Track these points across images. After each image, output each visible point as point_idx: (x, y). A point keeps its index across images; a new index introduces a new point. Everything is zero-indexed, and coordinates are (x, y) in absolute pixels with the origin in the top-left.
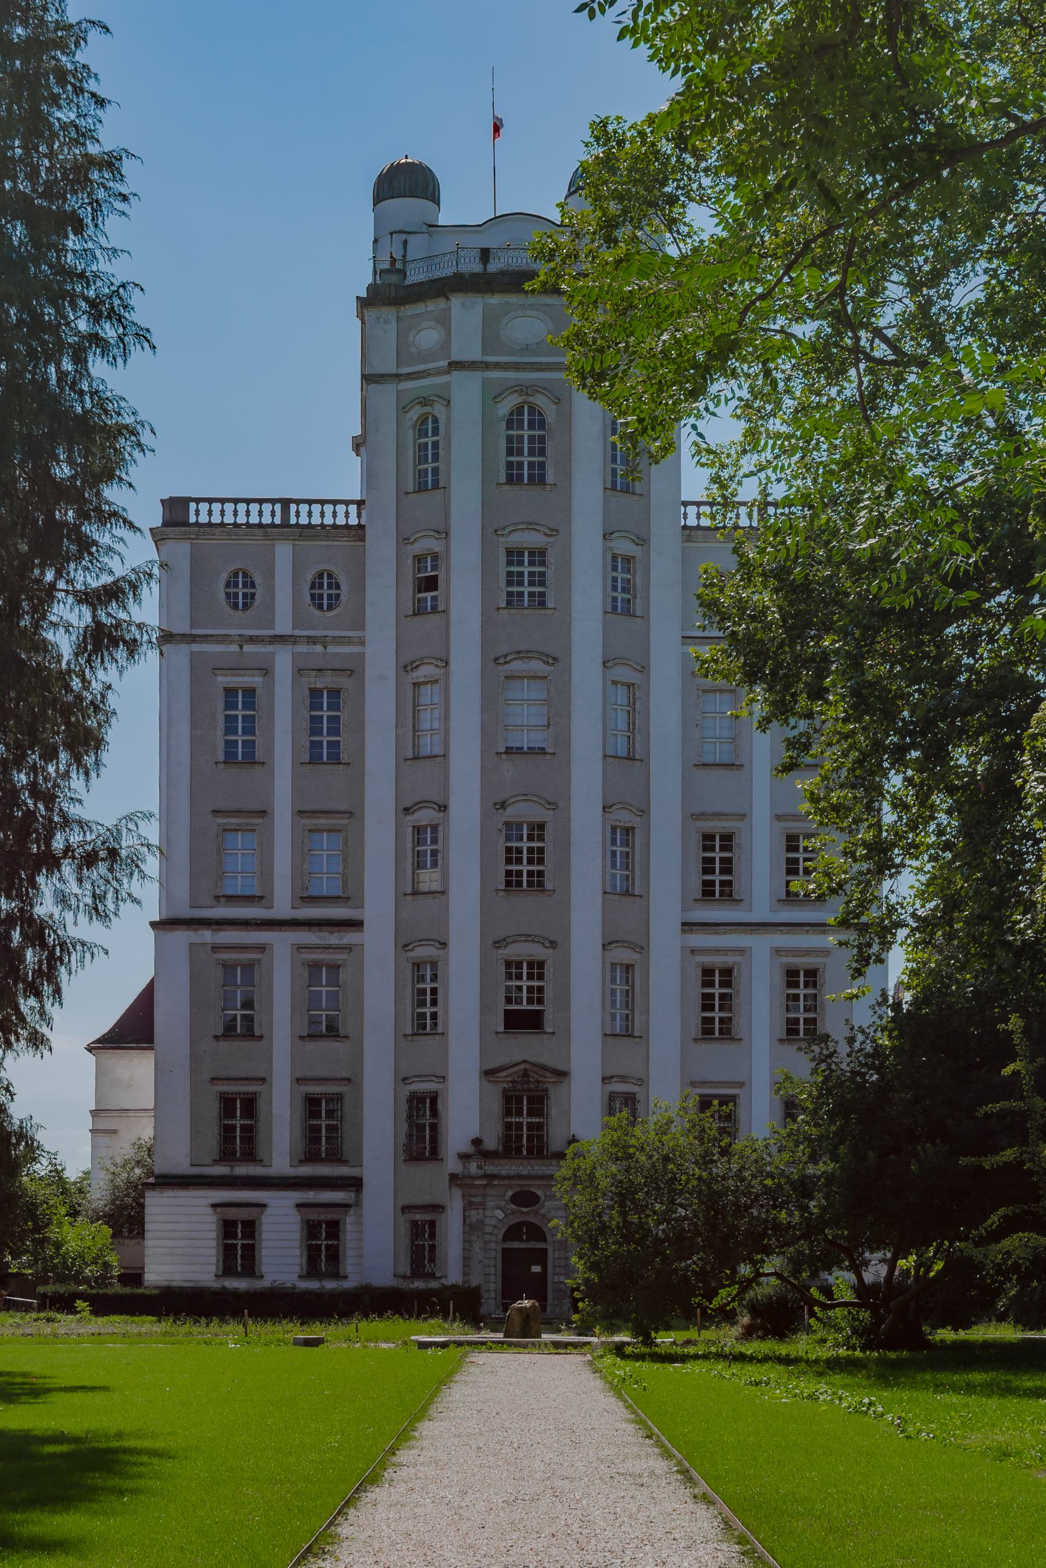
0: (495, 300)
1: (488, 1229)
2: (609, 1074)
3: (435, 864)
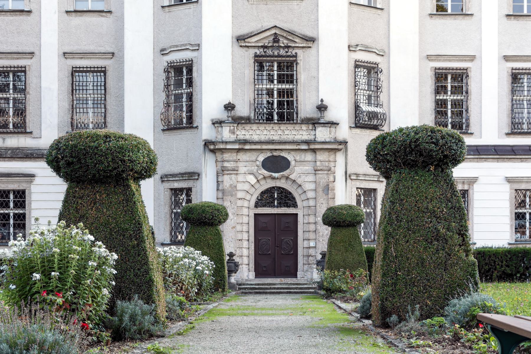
1: (240, 195)
2: (353, 43)
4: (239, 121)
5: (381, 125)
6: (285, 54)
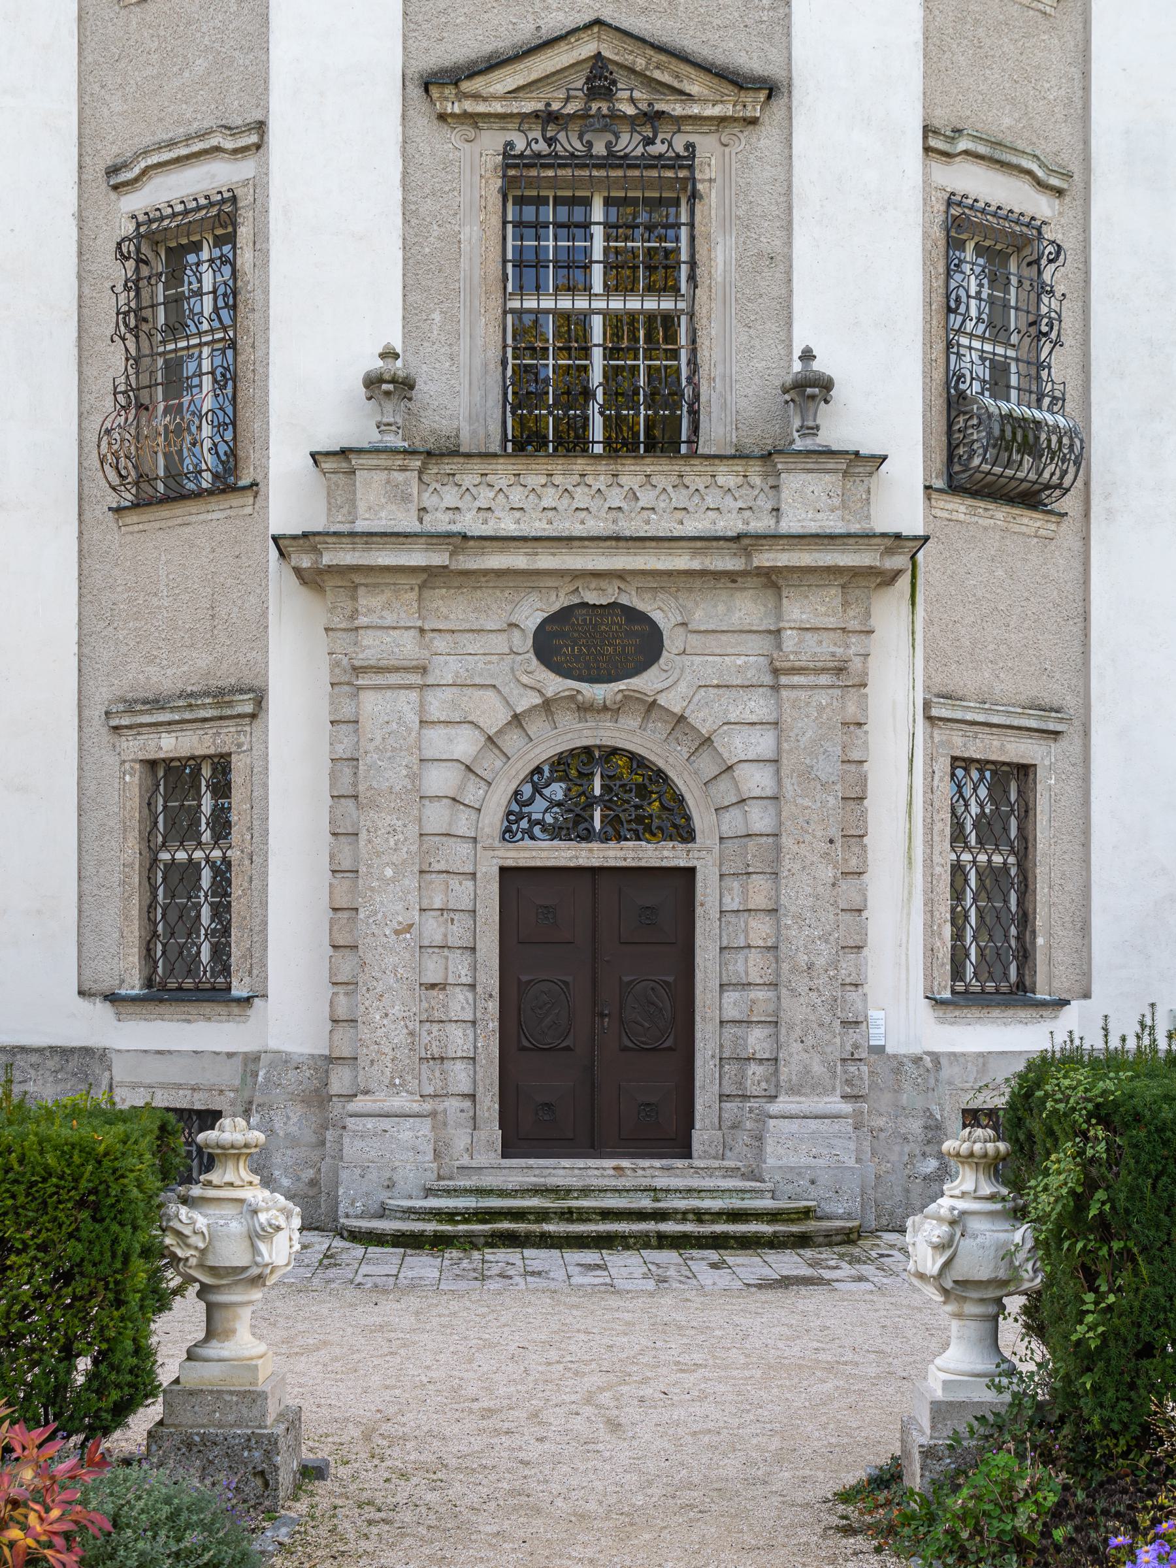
2: (943, 118)
5: (1059, 486)
6: (640, 151)
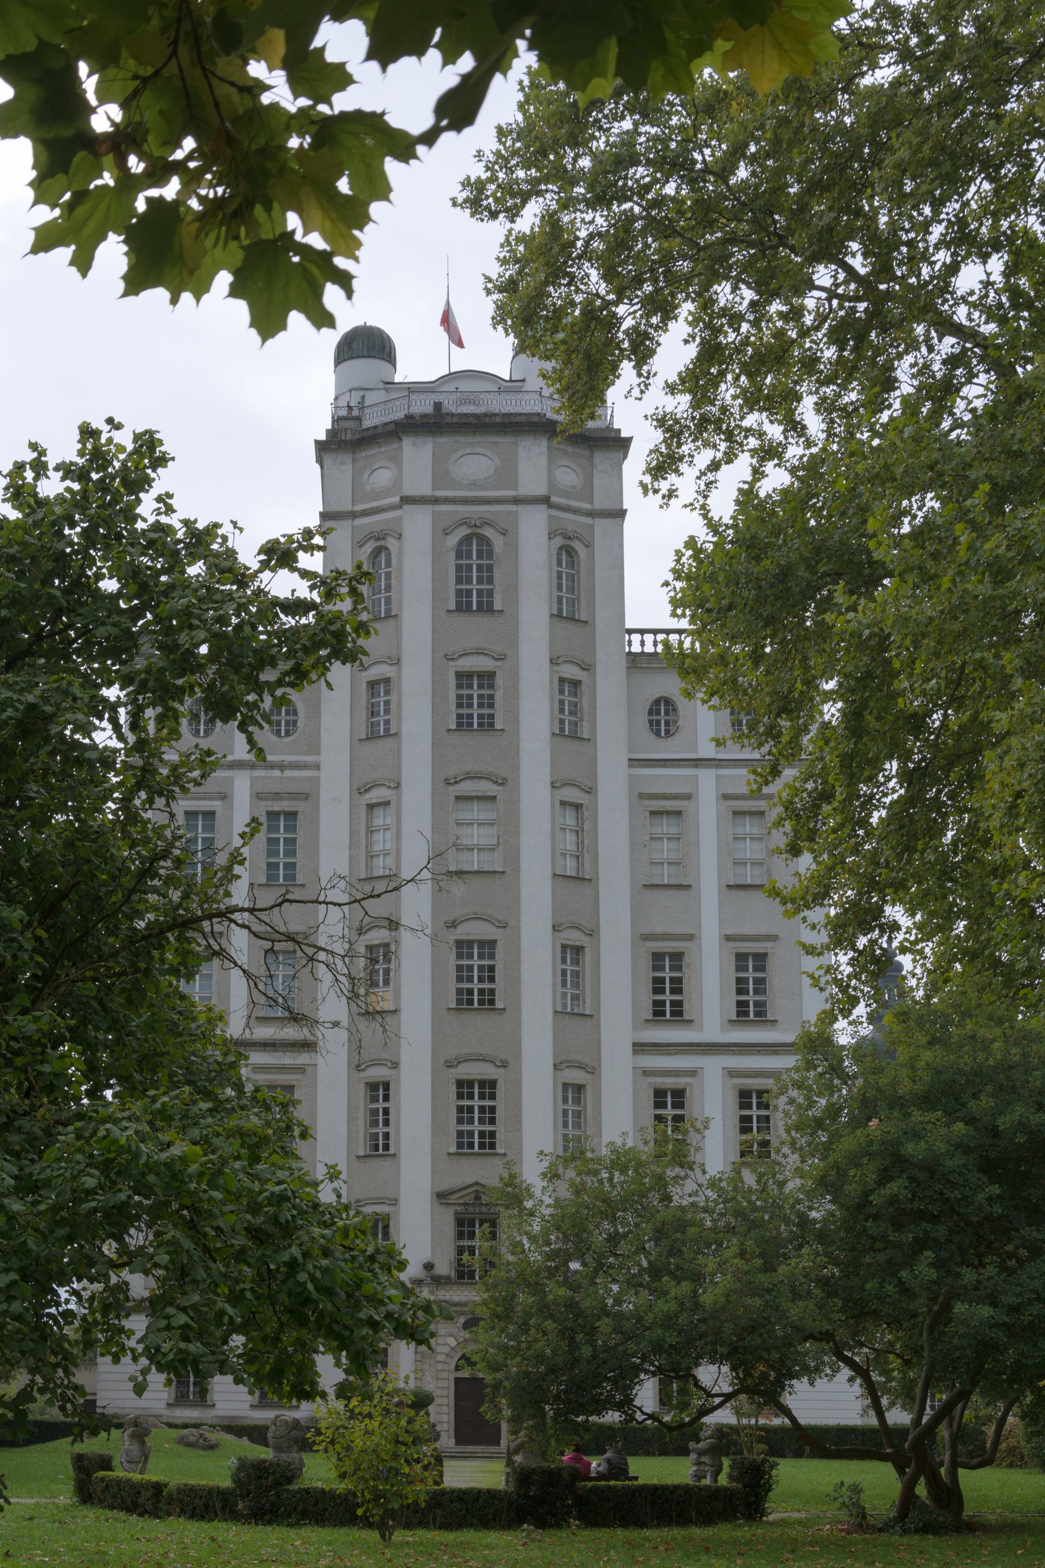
0: (444, 440)
3: (386, 982)
4: (439, 1281)
